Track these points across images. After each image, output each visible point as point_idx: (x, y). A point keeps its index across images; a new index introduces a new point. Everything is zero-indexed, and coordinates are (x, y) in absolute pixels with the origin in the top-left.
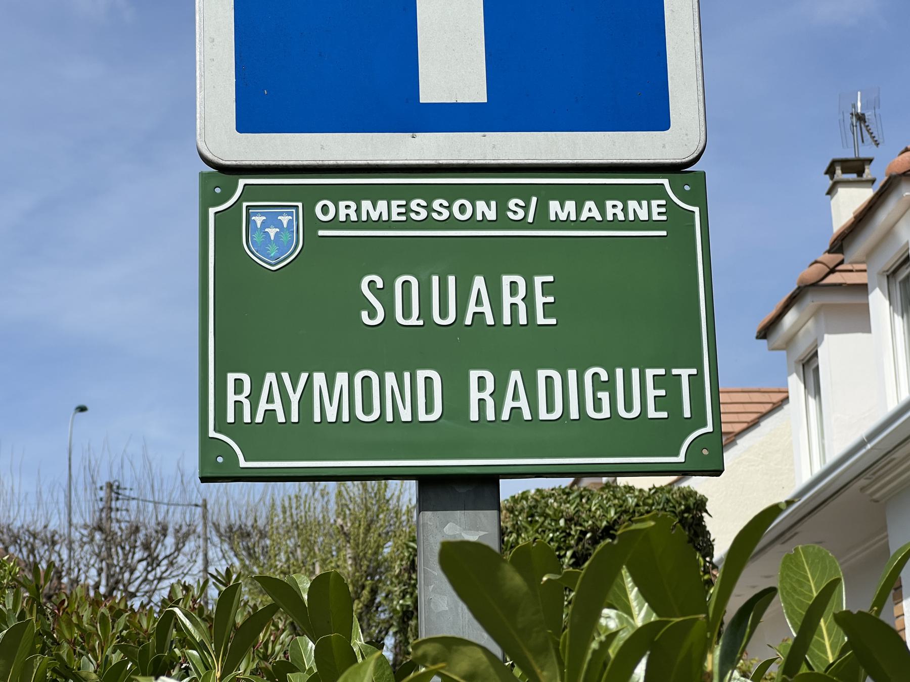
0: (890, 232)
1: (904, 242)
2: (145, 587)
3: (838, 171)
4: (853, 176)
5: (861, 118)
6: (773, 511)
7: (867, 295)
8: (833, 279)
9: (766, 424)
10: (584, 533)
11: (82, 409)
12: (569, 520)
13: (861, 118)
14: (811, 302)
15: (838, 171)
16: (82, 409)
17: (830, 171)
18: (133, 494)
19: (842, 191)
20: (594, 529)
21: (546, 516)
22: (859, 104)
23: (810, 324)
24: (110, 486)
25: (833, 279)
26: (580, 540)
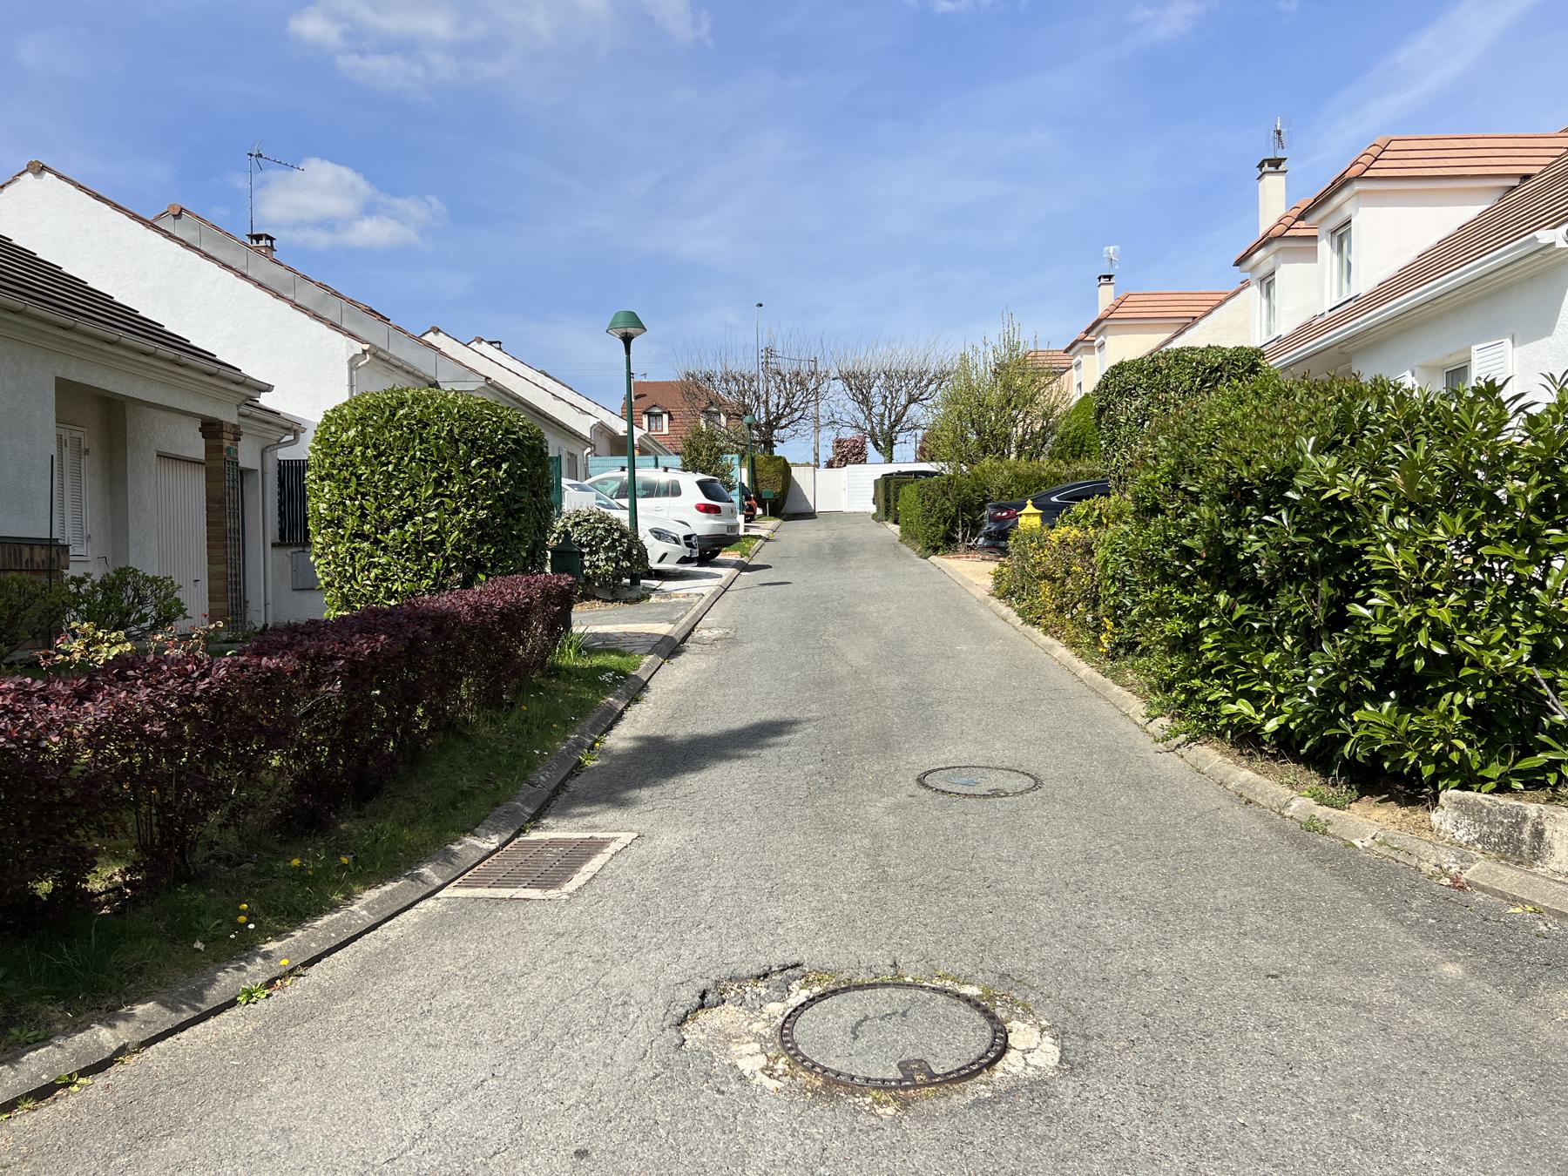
0: (1338, 208)
1: (1348, 214)
2: (802, 406)
3: (1266, 165)
4: (1273, 169)
5: (1279, 133)
6: (240, 370)
7: (1317, 241)
8: (1289, 233)
9: (1215, 312)
10: (1205, 369)
11: (761, 305)
12: (1198, 363)
13: (1279, 133)
14: (1275, 246)
15: (1266, 165)
16: (761, 305)
17: (1261, 166)
18: (778, 354)
19: (1267, 177)
20: (1211, 367)
21: (1185, 361)
22: (1279, 125)
23: (1271, 258)
24: (767, 349)
25: (1289, 233)
26: (1204, 373)
